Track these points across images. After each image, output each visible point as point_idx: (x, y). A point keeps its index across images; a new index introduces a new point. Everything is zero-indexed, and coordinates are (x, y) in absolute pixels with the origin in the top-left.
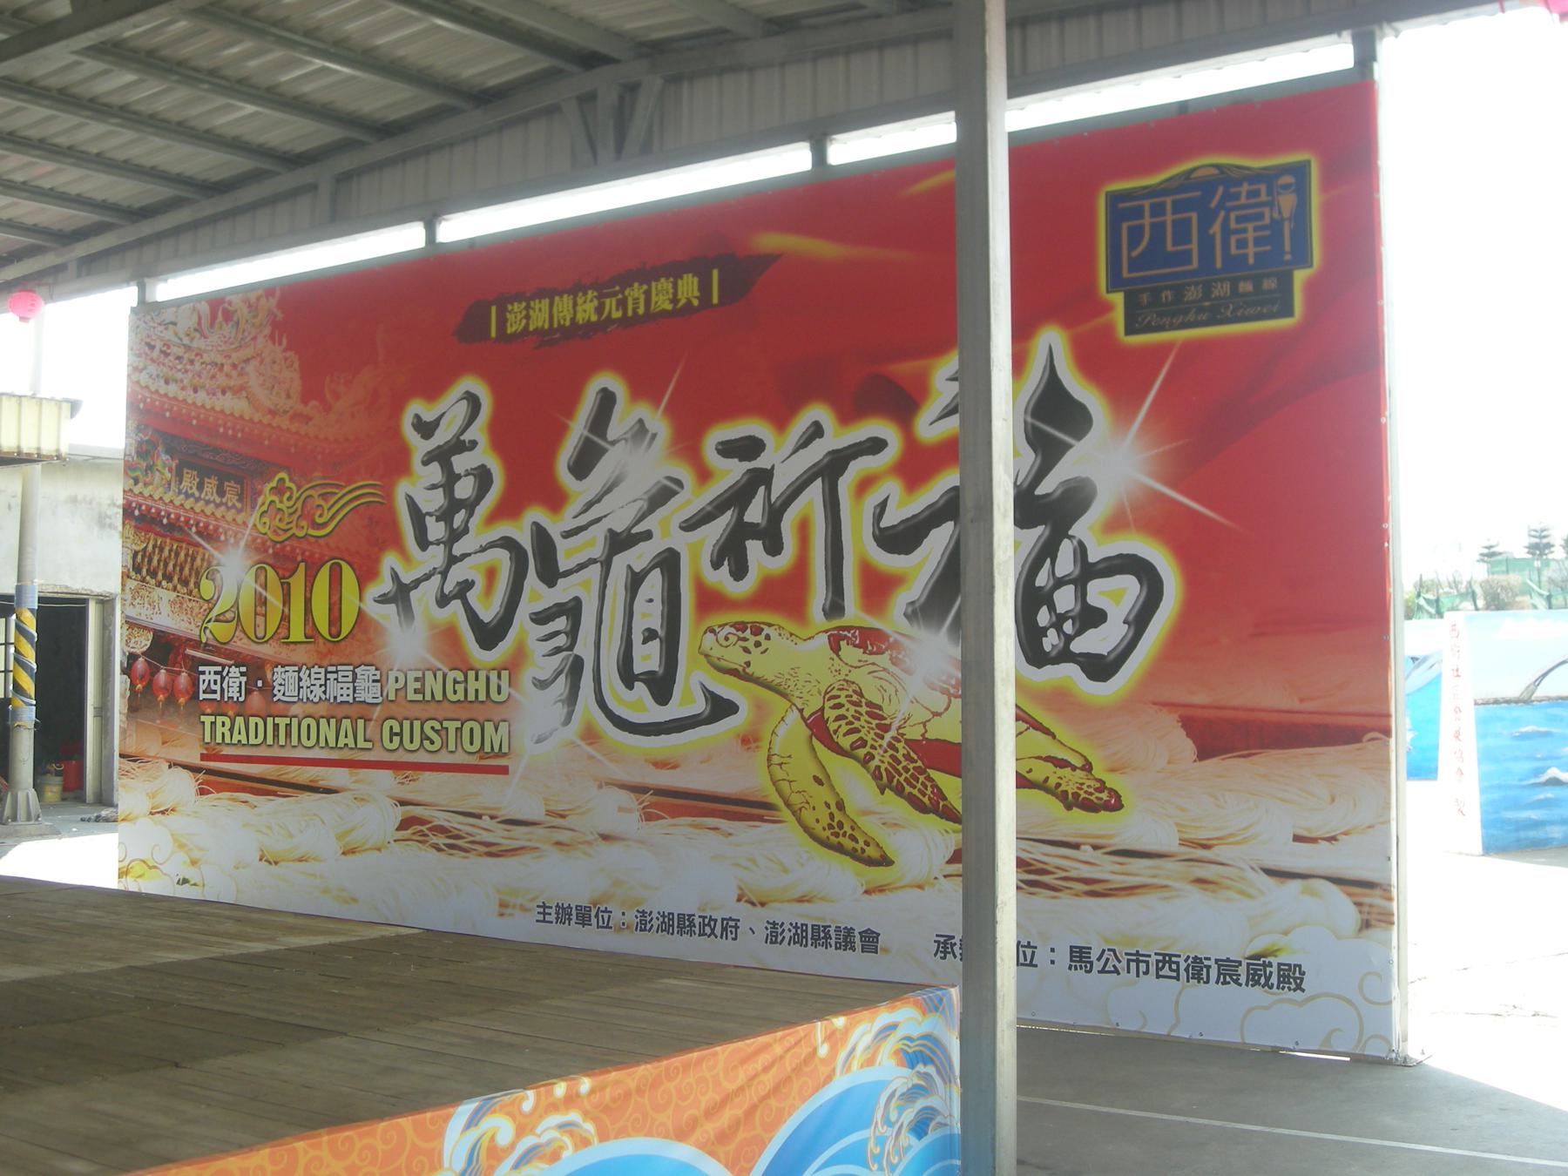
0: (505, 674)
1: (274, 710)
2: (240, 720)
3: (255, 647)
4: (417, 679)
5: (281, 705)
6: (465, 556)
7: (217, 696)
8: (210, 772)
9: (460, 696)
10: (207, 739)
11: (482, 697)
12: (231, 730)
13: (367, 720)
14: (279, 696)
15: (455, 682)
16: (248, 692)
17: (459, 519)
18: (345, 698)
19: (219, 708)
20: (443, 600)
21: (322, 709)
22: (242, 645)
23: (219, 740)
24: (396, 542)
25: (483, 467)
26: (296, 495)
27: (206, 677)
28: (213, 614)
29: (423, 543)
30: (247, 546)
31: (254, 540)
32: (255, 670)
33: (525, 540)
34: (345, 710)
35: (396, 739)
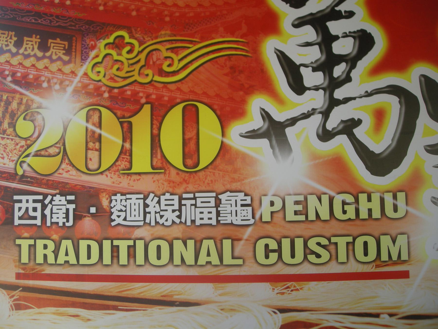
0: (401, 196)
1: (111, 233)
2: (67, 244)
3: (85, 178)
4: (297, 203)
5: (122, 229)
6: (347, 100)
7: (38, 222)
8: (26, 289)
9: (351, 214)
10: (25, 259)
11: (376, 214)
12: (56, 253)
13: (234, 240)
14: (120, 221)
15: (344, 203)
16: (77, 217)
17: (339, 70)
18: (206, 221)
19: (41, 232)
20: (325, 135)
21: (177, 231)
22: (69, 176)
23: (40, 259)
24: (266, 86)
25: (363, 32)
26: (137, 49)
27: (24, 205)
28: (33, 149)
29: (298, 87)
30: (76, 91)
31: (85, 86)
32: (86, 200)
33: (415, 88)
34: (207, 232)
35: (274, 257)
